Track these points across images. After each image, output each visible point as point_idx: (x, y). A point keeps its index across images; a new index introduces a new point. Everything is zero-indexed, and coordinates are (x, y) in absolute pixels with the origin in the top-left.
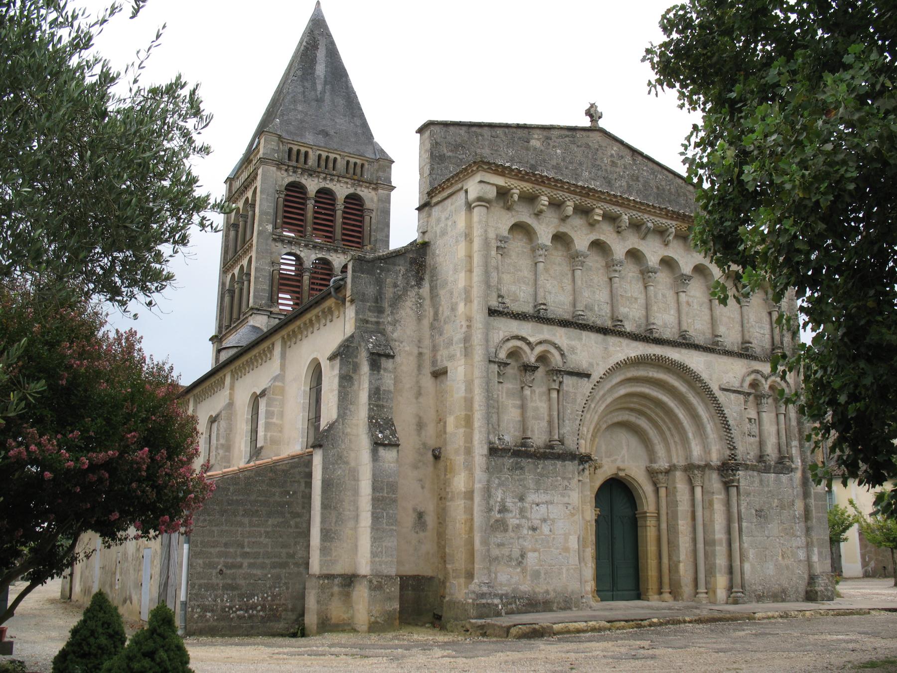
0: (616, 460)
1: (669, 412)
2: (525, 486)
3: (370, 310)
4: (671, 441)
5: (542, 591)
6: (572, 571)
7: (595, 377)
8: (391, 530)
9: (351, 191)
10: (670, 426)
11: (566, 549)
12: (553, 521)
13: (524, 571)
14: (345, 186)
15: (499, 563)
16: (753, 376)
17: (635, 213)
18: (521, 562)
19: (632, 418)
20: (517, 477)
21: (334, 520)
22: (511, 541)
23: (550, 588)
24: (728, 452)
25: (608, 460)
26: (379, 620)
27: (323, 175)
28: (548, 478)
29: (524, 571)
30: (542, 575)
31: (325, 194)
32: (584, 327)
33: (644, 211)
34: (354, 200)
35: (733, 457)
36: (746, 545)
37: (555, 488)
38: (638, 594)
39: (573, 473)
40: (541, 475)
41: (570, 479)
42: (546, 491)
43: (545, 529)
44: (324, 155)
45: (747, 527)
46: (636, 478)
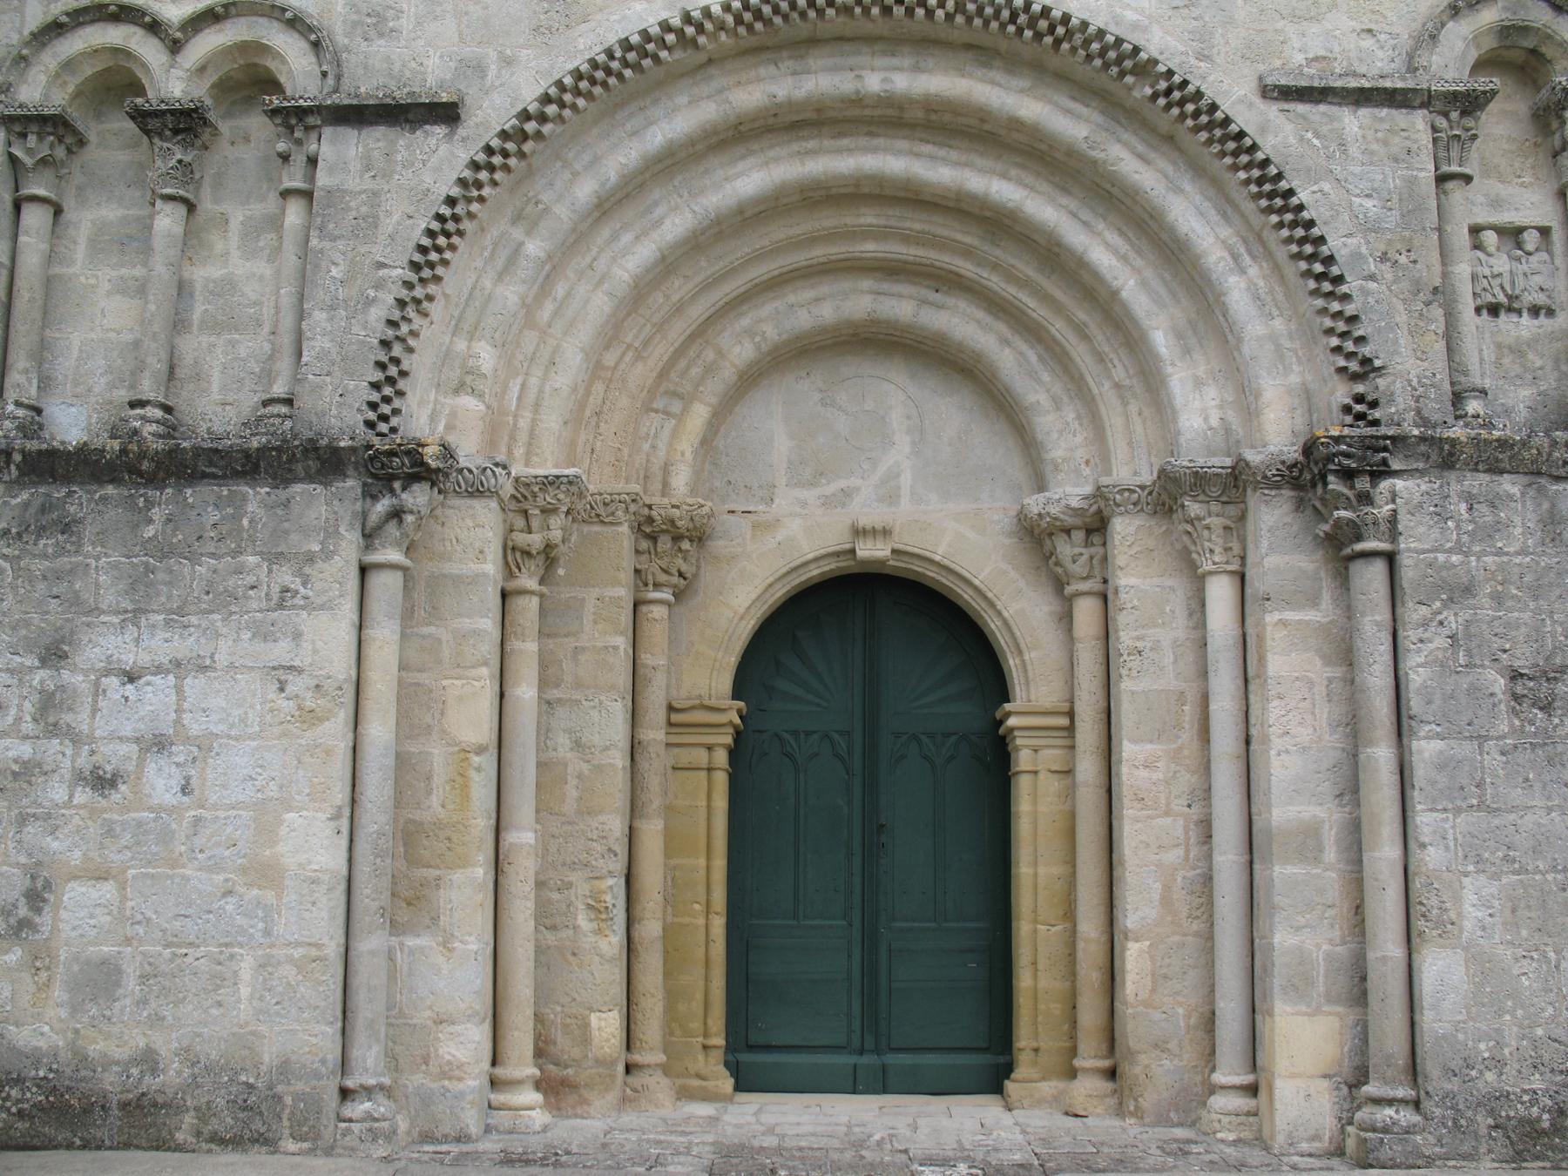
0: (847, 494)
1: (1053, 256)
2: (75, 601)
4: (1103, 391)
6: (289, 972)
7: (490, 114)
10: (1081, 315)
11: (267, 874)
12: (204, 746)
13: (40, 960)
18: (24, 924)
19: (902, 306)
20: (39, 566)
23: (165, 1044)
24: (1342, 393)
25: (810, 495)
30: (131, 984)
35: (1362, 409)
36: (1432, 858)
37: (223, 600)
38: (992, 1073)
39: (331, 532)
40: (164, 551)
41: (310, 558)
42: (177, 616)
43: (161, 782)
46: (964, 565)
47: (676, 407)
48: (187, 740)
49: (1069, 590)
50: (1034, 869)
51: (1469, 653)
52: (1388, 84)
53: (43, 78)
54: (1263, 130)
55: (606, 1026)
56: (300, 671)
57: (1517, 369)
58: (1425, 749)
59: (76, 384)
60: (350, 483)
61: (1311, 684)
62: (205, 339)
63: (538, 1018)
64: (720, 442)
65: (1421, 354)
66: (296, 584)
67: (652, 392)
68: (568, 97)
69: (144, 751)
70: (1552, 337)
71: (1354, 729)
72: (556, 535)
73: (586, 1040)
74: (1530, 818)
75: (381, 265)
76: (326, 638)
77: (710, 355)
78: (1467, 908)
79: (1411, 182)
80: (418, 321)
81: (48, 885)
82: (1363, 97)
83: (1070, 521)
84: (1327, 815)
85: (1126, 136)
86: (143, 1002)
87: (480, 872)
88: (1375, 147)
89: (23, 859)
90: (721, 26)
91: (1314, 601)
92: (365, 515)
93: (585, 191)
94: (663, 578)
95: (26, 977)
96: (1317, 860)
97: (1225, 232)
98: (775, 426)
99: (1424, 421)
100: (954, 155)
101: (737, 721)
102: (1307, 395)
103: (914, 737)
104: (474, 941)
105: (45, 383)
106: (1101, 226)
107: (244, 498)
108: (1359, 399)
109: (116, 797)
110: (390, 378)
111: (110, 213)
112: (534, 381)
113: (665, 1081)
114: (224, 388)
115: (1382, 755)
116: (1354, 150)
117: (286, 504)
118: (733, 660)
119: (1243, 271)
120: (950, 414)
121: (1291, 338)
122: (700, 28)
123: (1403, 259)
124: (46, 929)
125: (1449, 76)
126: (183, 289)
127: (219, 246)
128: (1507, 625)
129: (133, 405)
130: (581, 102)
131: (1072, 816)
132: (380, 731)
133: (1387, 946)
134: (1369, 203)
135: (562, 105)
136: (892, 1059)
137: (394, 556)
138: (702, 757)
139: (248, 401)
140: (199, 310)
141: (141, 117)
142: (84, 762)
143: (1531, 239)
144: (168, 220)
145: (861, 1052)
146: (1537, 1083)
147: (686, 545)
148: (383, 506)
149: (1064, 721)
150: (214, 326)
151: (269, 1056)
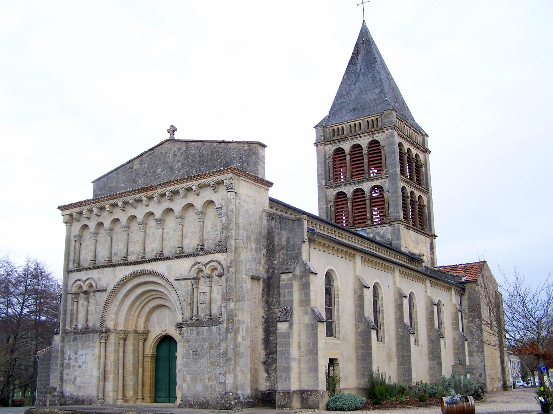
7: (109, 290)
9: (371, 139)
11: (92, 376)
12: (87, 362)
14: (366, 138)
16: (196, 267)
27: (350, 138)
30: (82, 388)
31: (357, 147)
34: (374, 144)
37: (89, 347)
43: (84, 367)
44: (352, 124)
76: (97, 351)
82: (184, 279)
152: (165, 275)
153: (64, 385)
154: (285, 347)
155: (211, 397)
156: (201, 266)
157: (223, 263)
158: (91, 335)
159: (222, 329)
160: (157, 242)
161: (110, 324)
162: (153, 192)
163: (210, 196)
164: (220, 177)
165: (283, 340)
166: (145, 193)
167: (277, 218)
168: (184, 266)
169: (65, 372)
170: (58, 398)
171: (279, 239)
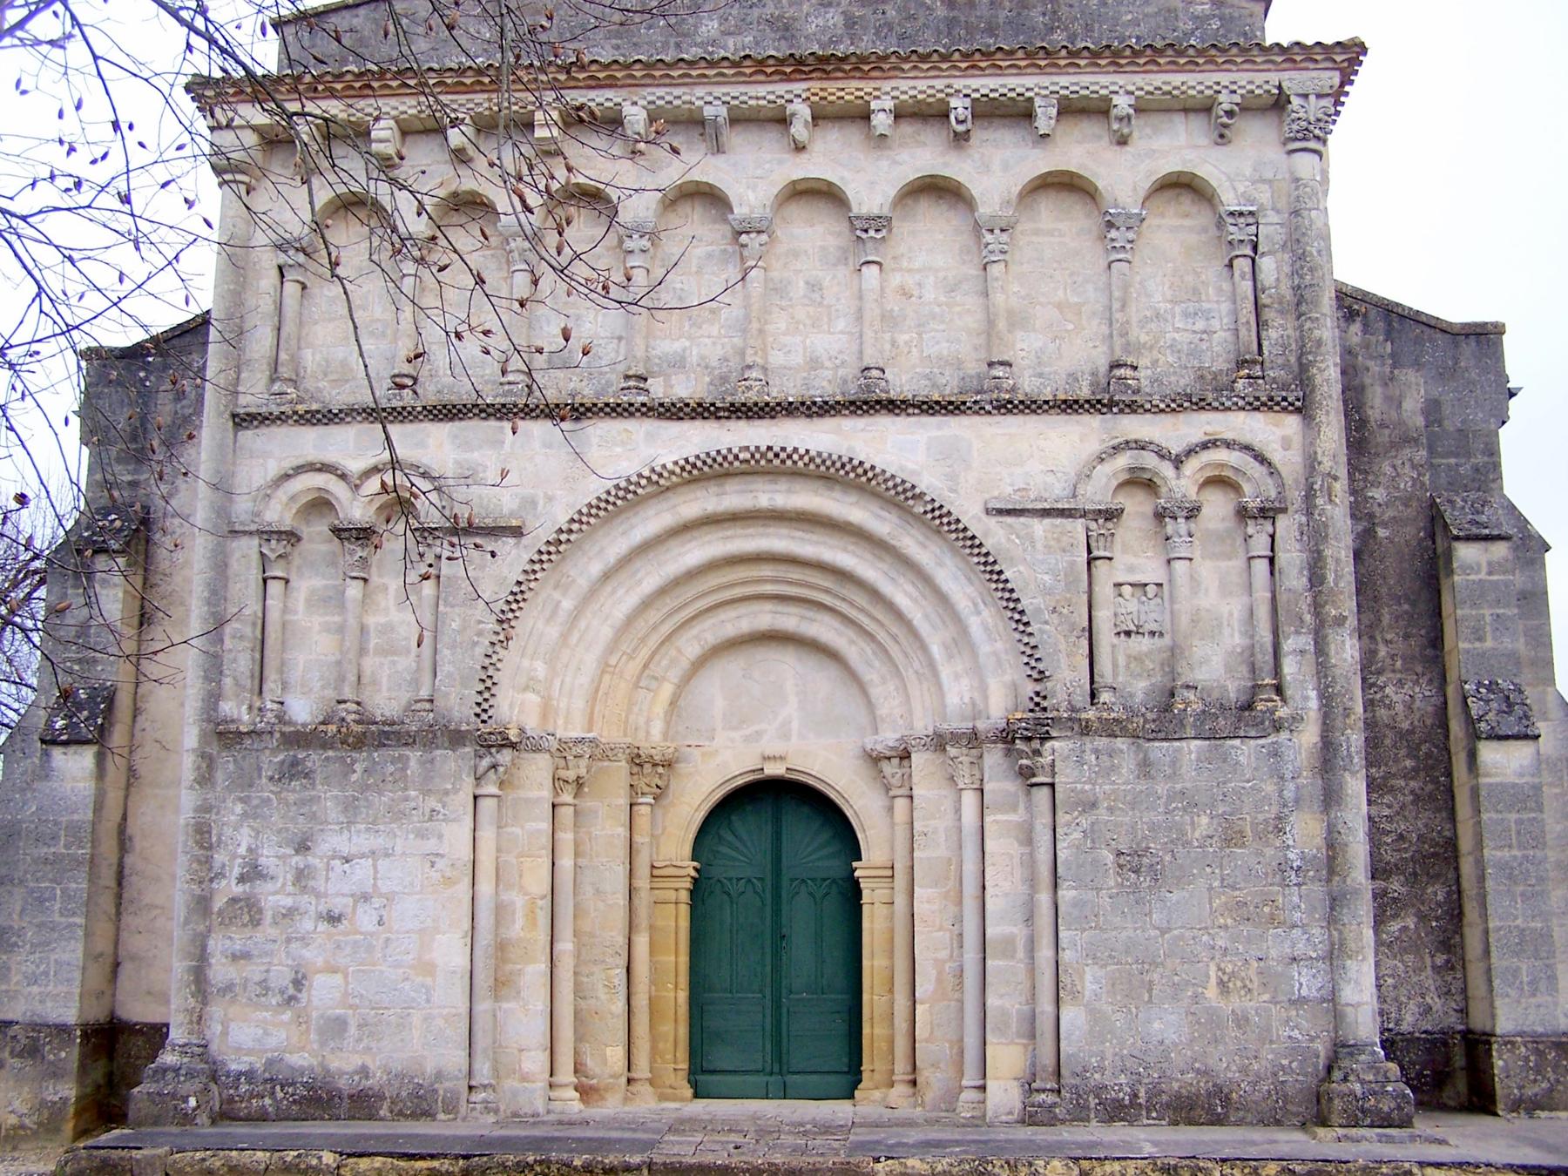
0: (759, 734)
3: (119, 460)
4: (909, 675)
5: (349, 1068)
6: (440, 1022)
7: (541, 532)
8: (70, 925)
10: (894, 630)
11: (429, 968)
12: (390, 898)
15: (233, 1000)
16: (1124, 460)
17: (661, 92)
19: (789, 620)
20: (292, 797)
21: (18, 908)
22: (269, 946)
24: (1030, 688)
25: (736, 735)
26: (27, 1121)
28: (380, 794)
29: (301, 1020)
30: (352, 1030)
32: (893, 406)
33: (687, 81)
36: (1067, 956)
37: (399, 816)
39: (457, 777)
41: (447, 793)
43: (366, 919)
45: (1076, 904)
47: (654, 684)
48: (381, 895)
49: (892, 793)
50: (873, 963)
51: (1093, 841)
52: (1060, 506)
53: (279, 507)
54: (986, 534)
55: (616, 1055)
56: (442, 856)
57: (1138, 670)
58: (1066, 894)
59: (302, 686)
60: (467, 749)
61: (1012, 858)
62: (377, 660)
63: (576, 1053)
64: (681, 703)
65: (1074, 669)
66: (439, 807)
67: (639, 678)
68: (584, 519)
69: (356, 902)
70: (1160, 650)
71: (1032, 881)
72: (582, 772)
73: (605, 1062)
74: (1124, 934)
75: (480, 622)
76: (456, 837)
77: (673, 652)
78: (1087, 984)
79: (1073, 564)
80: (502, 653)
81: (304, 977)
83: (888, 754)
84: (1019, 931)
85: (913, 532)
86: (359, 1040)
87: (543, 967)
88: (1052, 543)
89: (290, 962)
90: (673, 473)
91: (1014, 809)
92: (476, 767)
93: (596, 568)
94: (646, 789)
95: (294, 1027)
96: (1013, 957)
97: (970, 590)
98: (717, 690)
99: (1073, 709)
100: (815, 537)
101: (693, 873)
102: (1015, 687)
103: (803, 881)
104: (540, 1004)
105: (285, 686)
106: (902, 580)
107: (408, 758)
108: (1038, 694)
109: (341, 927)
110: (488, 687)
111: (318, 582)
112: (568, 679)
113: (650, 1089)
114: (389, 689)
115: (1044, 898)
116: (1039, 546)
117: (432, 761)
118: (691, 836)
119: (979, 613)
120: (820, 679)
121: (1006, 652)
122: (660, 475)
123: (1065, 611)
124: (304, 1001)
125: (1097, 498)
126: (363, 629)
127: (383, 604)
128: (1116, 825)
129: (339, 702)
130: (592, 520)
131: (892, 930)
132: (486, 887)
133: (1046, 1006)
134: (1046, 578)
135: (581, 522)
136: (791, 1078)
137: (493, 790)
138: (672, 895)
139: (405, 696)
140: (373, 642)
141: (337, 531)
142: (323, 908)
143: (1151, 590)
144: (354, 590)
145: (771, 1074)
146: (1123, 1079)
147: (660, 770)
148: (486, 762)
149: (889, 873)
150: (383, 652)
151: (430, 1068)
152: (930, 482)
153: (216, 1010)
154: (1521, 846)
155: (1244, 1070)
156: (1149, 460)
157: (1276, 456)
158: (414, 756)
159: (1289, 755)
160: (841, 324)
161: (516, 708)
162: (868, 86)
163: (1190, 155)
164: (1274, 78)
165: (1513, 816)
166: (815, 86)
167: (1373, 313)
168: (1055, 454)
169: (216, 944)
170: (197, 1085)
171: (1388, 399)
